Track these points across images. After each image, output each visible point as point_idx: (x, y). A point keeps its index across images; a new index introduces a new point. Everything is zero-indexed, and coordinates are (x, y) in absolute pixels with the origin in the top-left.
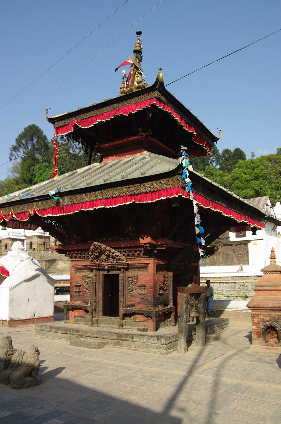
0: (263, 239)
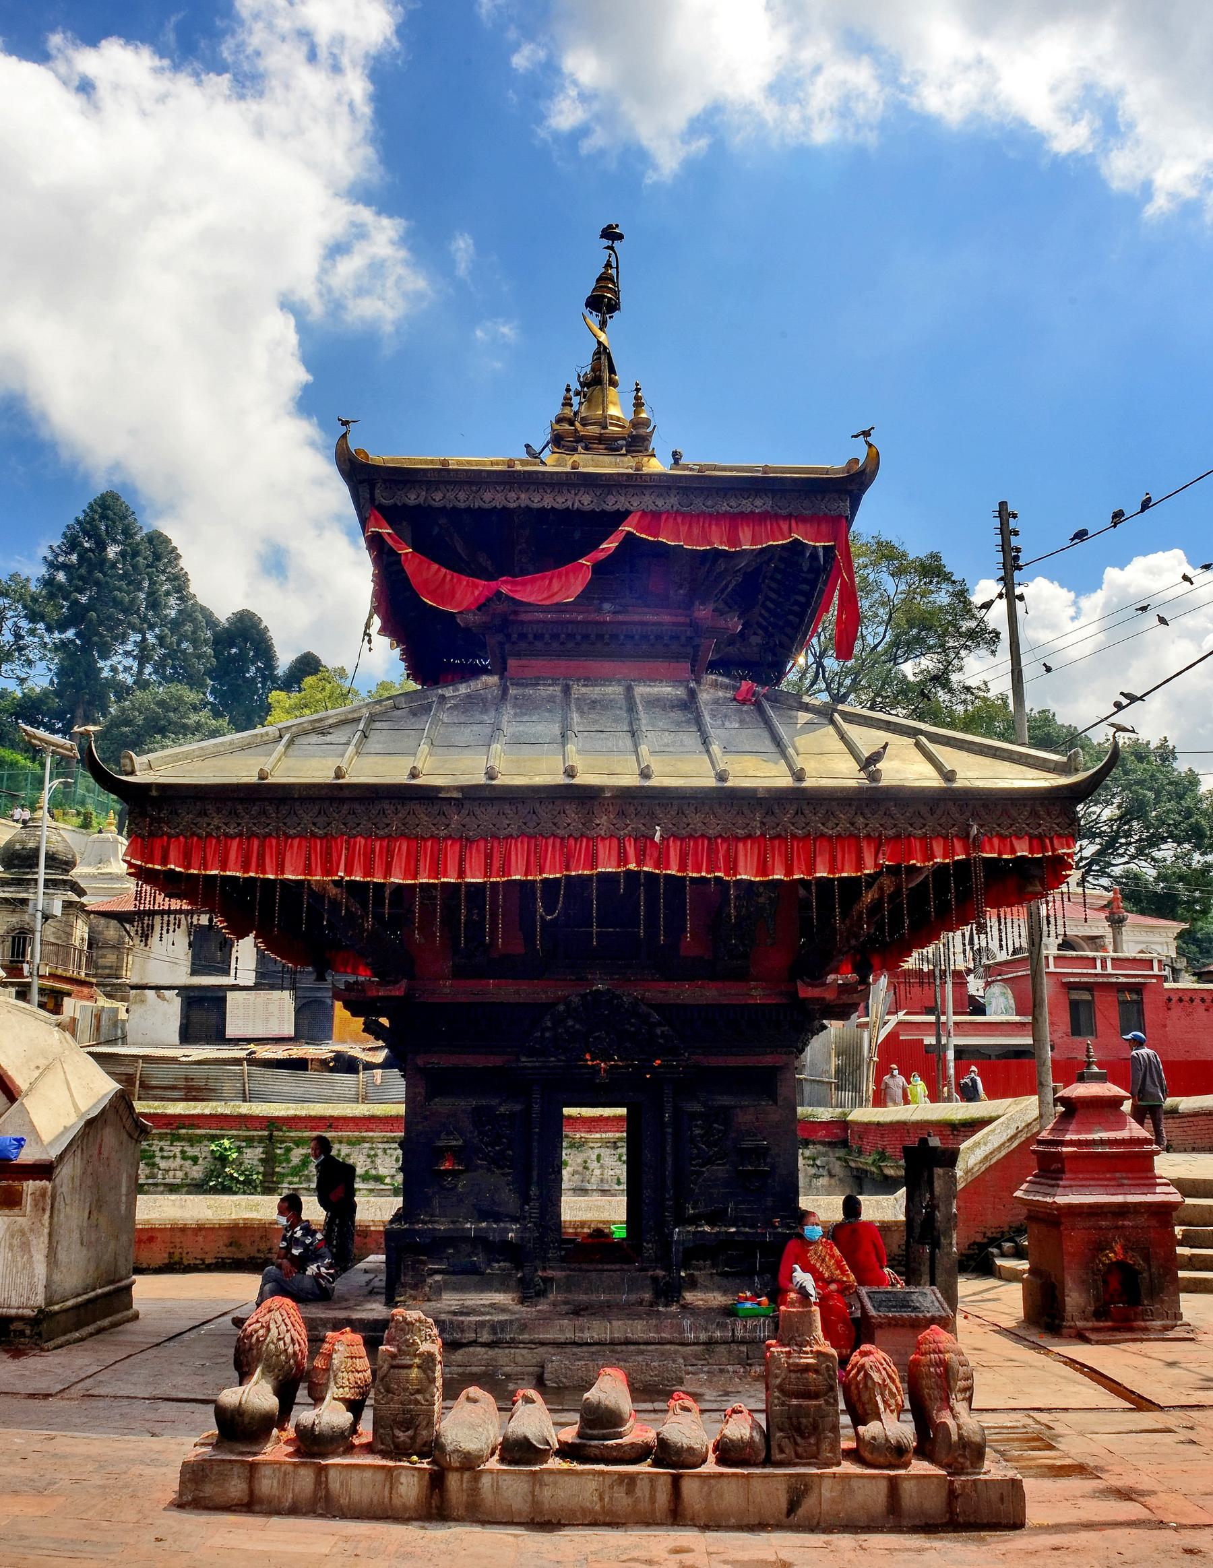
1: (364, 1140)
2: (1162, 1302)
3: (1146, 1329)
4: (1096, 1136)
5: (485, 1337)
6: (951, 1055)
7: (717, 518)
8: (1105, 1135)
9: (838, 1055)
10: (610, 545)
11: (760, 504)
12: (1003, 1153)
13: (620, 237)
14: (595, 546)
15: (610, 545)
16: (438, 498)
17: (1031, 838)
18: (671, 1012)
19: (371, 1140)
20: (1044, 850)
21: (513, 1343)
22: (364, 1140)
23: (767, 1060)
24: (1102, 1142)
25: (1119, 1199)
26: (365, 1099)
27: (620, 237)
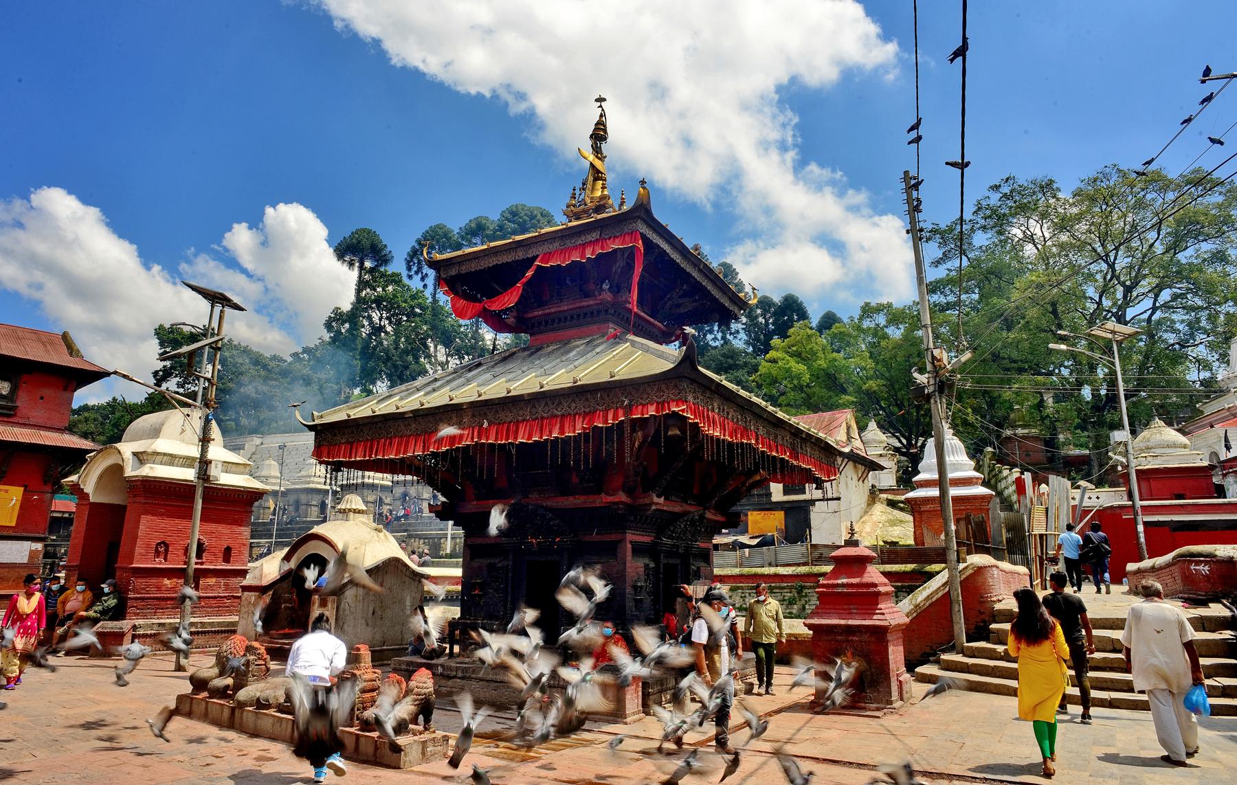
0: (839, 499)
1: (738, 588)
2: (879, 691)
3: (865, 709)
4: (839, 582)
5: (460, 675)
6: (1141, 528)
7: (575, 248)
8: (845, 581)
9: (1008, 531)
10: (529, 274)
11: (595, 236)
12: (940, 594)
13: (604, 100)
14: (523, 275)
15: (529, 274)
16: (464, 269)
17: (658, 404)
18: (559, 512)
19: (742, 588)
20: (663, 409)
21: (470, 678)
22: (738, 588)
23: (614, 537)
24: (843, 585)
25: (843, 622)
26: (741, 565)
27: (604, 100)
